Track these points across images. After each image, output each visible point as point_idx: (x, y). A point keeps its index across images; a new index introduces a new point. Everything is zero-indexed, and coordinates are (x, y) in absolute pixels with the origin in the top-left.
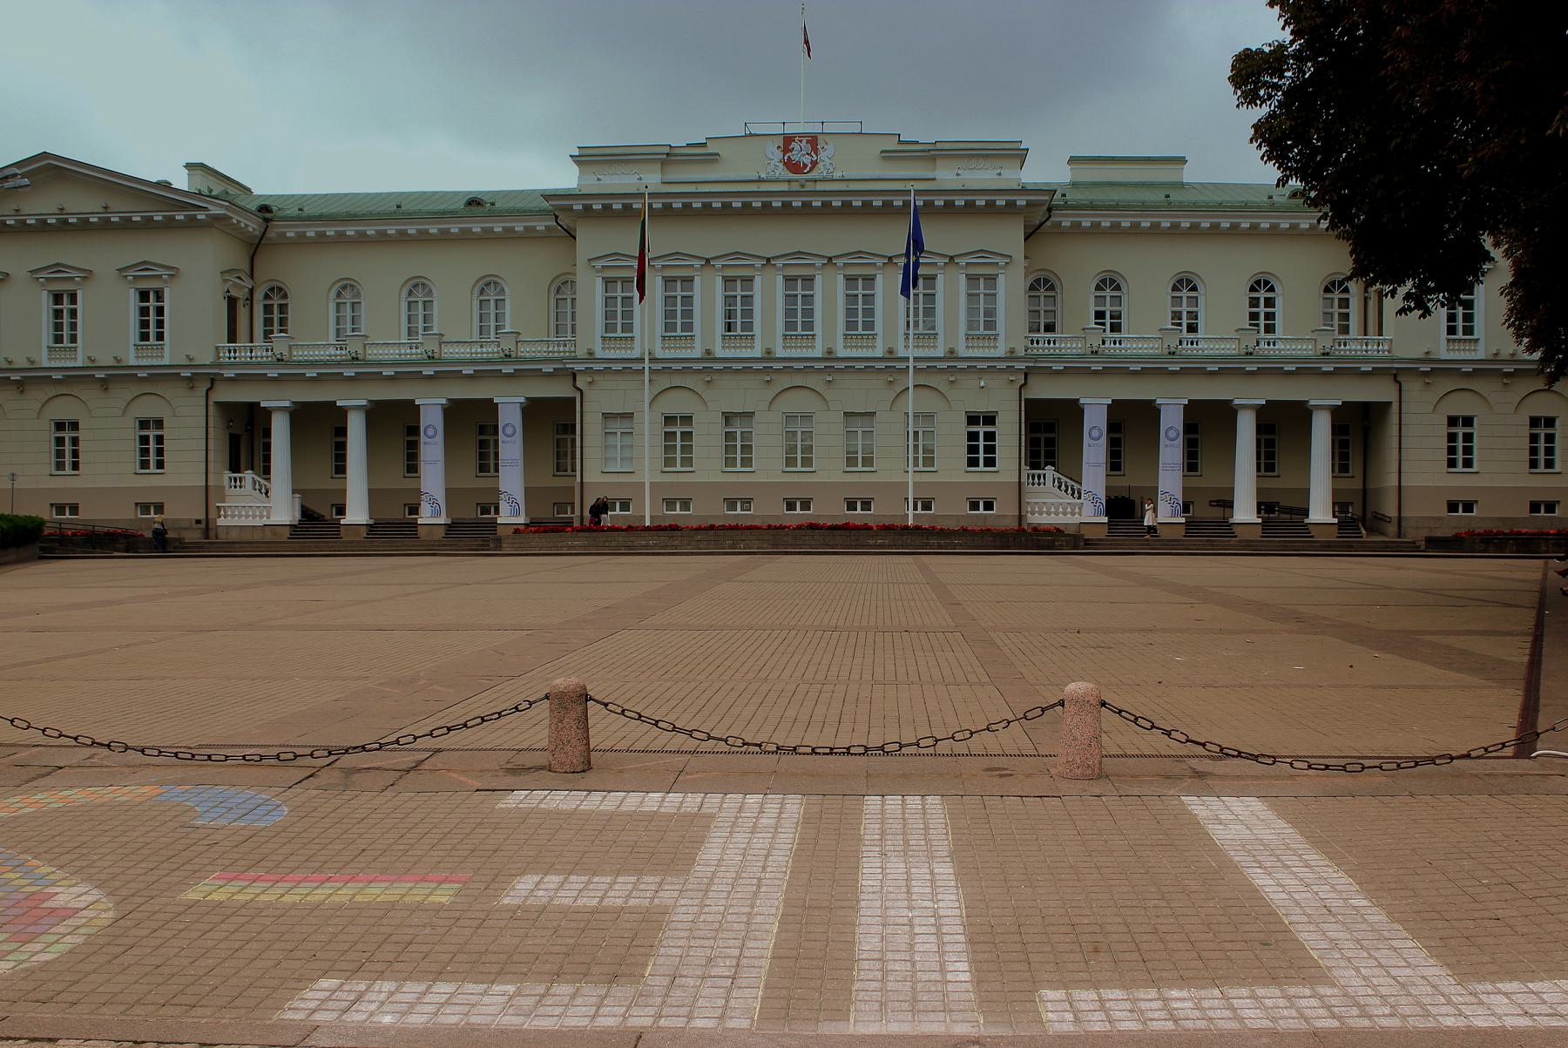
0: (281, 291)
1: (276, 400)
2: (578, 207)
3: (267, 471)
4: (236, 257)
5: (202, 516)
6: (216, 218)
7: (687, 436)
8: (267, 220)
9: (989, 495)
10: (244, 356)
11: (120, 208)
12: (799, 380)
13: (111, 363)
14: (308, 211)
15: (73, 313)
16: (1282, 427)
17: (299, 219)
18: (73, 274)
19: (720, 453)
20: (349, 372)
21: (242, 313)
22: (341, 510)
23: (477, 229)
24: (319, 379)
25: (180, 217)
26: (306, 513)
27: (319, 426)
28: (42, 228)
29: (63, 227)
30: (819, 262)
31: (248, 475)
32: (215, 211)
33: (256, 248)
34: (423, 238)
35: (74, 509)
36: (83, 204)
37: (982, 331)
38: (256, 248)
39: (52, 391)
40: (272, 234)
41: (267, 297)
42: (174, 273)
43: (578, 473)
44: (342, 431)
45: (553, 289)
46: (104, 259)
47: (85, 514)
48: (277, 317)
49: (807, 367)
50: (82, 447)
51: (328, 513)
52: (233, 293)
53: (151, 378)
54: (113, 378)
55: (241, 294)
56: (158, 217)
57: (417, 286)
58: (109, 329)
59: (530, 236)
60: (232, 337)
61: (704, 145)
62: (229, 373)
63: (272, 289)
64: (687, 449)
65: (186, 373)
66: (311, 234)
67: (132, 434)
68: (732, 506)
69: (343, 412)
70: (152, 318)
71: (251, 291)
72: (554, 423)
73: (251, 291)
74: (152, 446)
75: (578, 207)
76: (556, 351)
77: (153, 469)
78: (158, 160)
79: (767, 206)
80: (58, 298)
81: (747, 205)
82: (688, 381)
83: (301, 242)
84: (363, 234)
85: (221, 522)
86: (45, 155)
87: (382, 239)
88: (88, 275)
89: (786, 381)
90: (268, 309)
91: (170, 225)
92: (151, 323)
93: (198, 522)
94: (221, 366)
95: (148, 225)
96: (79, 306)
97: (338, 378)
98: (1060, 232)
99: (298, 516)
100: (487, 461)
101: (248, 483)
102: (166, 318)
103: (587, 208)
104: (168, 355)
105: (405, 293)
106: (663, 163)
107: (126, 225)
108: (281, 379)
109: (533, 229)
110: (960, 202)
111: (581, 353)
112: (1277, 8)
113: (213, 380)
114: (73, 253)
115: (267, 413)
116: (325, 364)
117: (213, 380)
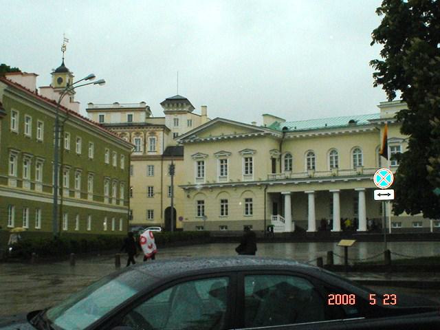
0: (289, 155)
1: (286, 191)
2: (379, 123)
3: (282, 214)
4: (274, 145)
6: (267, 134)
8: (284, 133)
10: (278, 177)
11: (239, 133)
13: (237, 181)
14: (298, 128)
15: (203, 167)
16: (324, 198)
17: (295, 131)
18: (203, 156)
20: (333, 180)
26: (297, 228)
27: (299, 199)
28: (218, 140)
29: (223, 140)
30: (401, 141)
31: (278, 216)
32: (266, 132)
33: (281, 142)
34: (334, 135)
35: (203, 228)
36: (228, 132)
38: (281, 142)
40: (286, 137)
41: (286, 157)
42: (255, 152)
43: (383, 213)
44: (332, 200)
46: (235, 148)
47: (229, 229)
48: (289, 166)
50: (253, 207)
51: (300, 225)
52: (274, 157)
53: (224, 187)
54: (239, 186)
55: (277, 157)
57: (356, 150)
58: (236, 172)
59: (368, 132)
60: (274, 171)
62: (271, 183)
65: (258, 184)
67: (219, 205)
68: (395, 225)
69: (357, 192)
70: (249, 166)
71: (281, 156)
73: (281, 156)
75: (379, 123)
77: (249, 214)
78: (251, 116)
83: (295, 139)
84: (307, 136)
86: (218, 118)
88: (230, 154)
90: (286, 161)
91: (253, 137)
92: (249, 169)
93: (262, 231)
95: (247, 138)
96: (253, 162)
98: (289, 140)
101: (278, 218)
102: (253, 166)
103: (389, 123)
104: (253, 179)
105: (329, 154)
107: (241, 138)
112: (380, 47)
113: (267, 186)
114: (227, 147)
117: (267, 186)
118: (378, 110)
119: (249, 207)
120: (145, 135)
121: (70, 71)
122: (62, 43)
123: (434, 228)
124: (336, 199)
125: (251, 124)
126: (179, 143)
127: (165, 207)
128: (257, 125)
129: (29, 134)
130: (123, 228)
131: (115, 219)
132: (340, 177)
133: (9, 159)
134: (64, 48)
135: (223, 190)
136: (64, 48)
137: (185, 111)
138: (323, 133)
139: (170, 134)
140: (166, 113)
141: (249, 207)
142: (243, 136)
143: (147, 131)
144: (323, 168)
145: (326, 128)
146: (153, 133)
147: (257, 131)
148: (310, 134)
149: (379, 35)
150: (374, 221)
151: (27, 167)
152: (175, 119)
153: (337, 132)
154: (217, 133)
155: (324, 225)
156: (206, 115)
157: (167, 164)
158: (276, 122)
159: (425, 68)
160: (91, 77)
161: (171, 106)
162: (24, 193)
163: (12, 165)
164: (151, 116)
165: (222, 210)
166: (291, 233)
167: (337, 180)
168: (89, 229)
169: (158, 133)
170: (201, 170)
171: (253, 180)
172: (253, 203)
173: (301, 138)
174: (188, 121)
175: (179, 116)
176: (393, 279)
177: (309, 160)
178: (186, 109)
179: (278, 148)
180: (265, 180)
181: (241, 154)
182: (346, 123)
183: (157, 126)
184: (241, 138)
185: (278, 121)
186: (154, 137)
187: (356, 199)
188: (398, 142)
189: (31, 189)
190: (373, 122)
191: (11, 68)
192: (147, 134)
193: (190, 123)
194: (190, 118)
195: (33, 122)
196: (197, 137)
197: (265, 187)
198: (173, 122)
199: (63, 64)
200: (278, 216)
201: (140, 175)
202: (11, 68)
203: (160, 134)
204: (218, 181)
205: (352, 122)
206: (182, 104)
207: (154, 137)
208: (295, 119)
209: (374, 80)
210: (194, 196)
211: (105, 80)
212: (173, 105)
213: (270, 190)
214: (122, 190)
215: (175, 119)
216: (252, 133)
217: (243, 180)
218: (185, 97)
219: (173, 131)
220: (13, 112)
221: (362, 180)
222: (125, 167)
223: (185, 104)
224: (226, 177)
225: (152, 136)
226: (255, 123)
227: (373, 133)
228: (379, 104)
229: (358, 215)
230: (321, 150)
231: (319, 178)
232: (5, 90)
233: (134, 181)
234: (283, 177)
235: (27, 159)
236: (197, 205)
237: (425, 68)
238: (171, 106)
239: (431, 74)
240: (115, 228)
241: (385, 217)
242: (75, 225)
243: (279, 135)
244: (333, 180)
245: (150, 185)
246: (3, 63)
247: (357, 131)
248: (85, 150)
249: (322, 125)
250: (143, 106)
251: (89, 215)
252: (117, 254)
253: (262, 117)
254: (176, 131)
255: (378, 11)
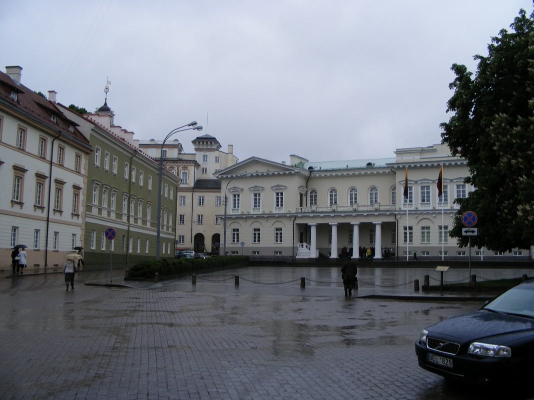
0: (314, 191)
1: (312, 223)
2: (396, 166)
3: (308, 241)
5: (292, 255)
7: (428, 233)
8: (311, 172)
9: (258, 250)
10: (304, 210)
11: (272, 171)
12: (425, 216)
14: (350, 167)
16: (324, 229)
18: (260, 189)
19: (420, 238)
21: (304, 198)
22: (330, 255)
23: (369, 173)
24: (324, 217)
25: (287, 172)
26: (321, 255)
27: (324, 229)
28: (252, 176)
29: (257, 176)
30: (431, 182)
31: (305, 244)
32: (296, 171)
33: (308, 179)
34: (354, 176)
36: (262, 170)
37: (426, 202)
38: (308, 179)
39: (254, 220)
40: (312, 175)
41: (311, 193)
42: (286, 187)
44: (331, 231)
45: (391, 190)
46: (267, 185)
47: (261, 254)
48: (314, 200)
49: (428, 212)
51: (325, 254)
52: (302, 192)
53: (257, 218)
54: (270, 216)
55: (304, 193)
56: (281, 173)
57: (373, 188)
58: (268, 204)
59: (384, 174)
60: (301, 205)
61: (432, 147)
62: (300, 215)
63: (312, 191)
64: (428, 237)
65: (288, 215)
66: (317, 175)
68: (424, 254)
71: (307, 192)
72: (390, 229)
73: (307, 192)
74: (279, 236)
76: (392, 208)
77: (279, 242)
78: (283, 158)
79: (450, 164)
80: (255, 195)
81: (427, 165)
82: (429, 217)
83: (320, 177)
84: (331, 175)
85: (297, 257)
86: (253, 157)
87: (343, 176)
88: (263, 189)
89: (421, 217)
90: (311, 196)
91: (285, 174)
92: (279, 202)
93: (291, 257)
94: (298, 213)
95: (279, 175)
97: (329, 216)
98: (315, 178)
99: (318, 256)
100: (372, 240)
102: (283, 200)
103: (398, 167)
104: (283, 211)
105: (349, 191)
106: (420, 152)
107: (273, 175)
108: (314, 217)
109: (385, 172)
110: (418, 165)
111: (398, 209)
113: (296, 217)
115: (310, 226)
116: (326, 212)
118: (395, 155)
119: (279, 236)
120: (178, 169)
121: (112, 110)
122: (104, 85)
123: (444, 257)
124: (334, 231)
125: (281, 163)
126: (218, 177)
127: (194, 234)
128: (286, 164)
129: (107, 168)
130: (171, 252)
131: (166, 244)
132: (338, 212)
133: (93, 190)
134: (107, 90)
135: (278, 220)
136: (107, 90)
137: (214, 149)
138: (339, 174)
139: (199, 169)
140: (196, 150)
141: (279, 235)
142: (276, 173)
143: (179, 167)
144: (343, 203)
145: (347, 170)
146: (185, 168)
147: (288, 170)
148: (334, 174)
149: (452, 104)
150: (385, 251)
151: (105, 196)
152: (204, 156)
153: (351, 173)
154: (252, 170)
155: (345, 253)
156: (232, 153)
157: (197, 195)
158: (301, 162)
159: (508, 136)
160: (194, 124)
161: (201, 143)
162: (103, 220)
163: (95, 195)
164: (182, 152)
165: (255, 238)
166: (316, 259)
167: (336, 214)
168: (147, 252)
169: (190, 168)
170: (237, 202)
171: (283, 212)
172: (283, 232)
173: (326, 177)
174: (216, 158)
175: (208, 153)
176: (446, 296)
177: (331, 196)
178: (214, 147)
179: (305, 185)
180: (294, 212)
181: (250, 190)
182: (364, 165)
183: (190, 161)
184: (273, 175)
185: (303, 161)
186: (186, 171)
187: (352, 231)
188: (429, 183)
189: (99, 214)
190: (389, 166)
191: (79, 108)
192: (180, 168)
193: (217, 159)
194: (217, 155)
195: (110, 156)
196: (235, 172)
197: (294, 219)
198: (202, 158)
199: (106, 104)
200: (305, 244)
201: (188, 204)
202: (79, 108)
203: (192, 168)
204: (252, 212)
205: (369, 164)
206: (211, 143)
207: (186, 171)
208: (320, 160)
209: (441, 139)
210: (230, 226)
211: (203, 127)
212: (203, 143)
213: (299, 221)
214: (171, 218)
215: (204, 156)
216: (283, 171)
217: (274, 212)
218: (214, 136)
219: (202, 166)
220: (97, 148)
221: (357, 216)
222: (173, 198)
223: (213, 143)
224: (239, 210)
225: (185, 170)
226: (285, 162)
227: (389, 174)
228: (396, 151)
229: (352, 245)
230: (343, 188)
231: (341, 212)
232: (93, 130)
233: (180, 210)
234: (309, 210)
235: (96, 186)
236: (233, 232)
237: (508, 136)
238: (201, 143)
239: (514, 141)
240: (165, 252)
241: (397, 247)
242: (137, 249)
243: (307, 174)
244: (332, 215)
245: (200, 213)
246: (73, 104)
247: (375, 172)
248: (146, 183)
249: (344, 166)
250: (176, 143)
251: (148, 239)
252: (194, 274)
253: (290, 157)
254: (205, 166)
255: (451, 86)
